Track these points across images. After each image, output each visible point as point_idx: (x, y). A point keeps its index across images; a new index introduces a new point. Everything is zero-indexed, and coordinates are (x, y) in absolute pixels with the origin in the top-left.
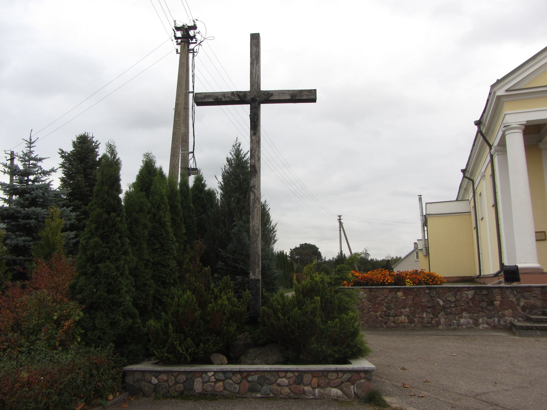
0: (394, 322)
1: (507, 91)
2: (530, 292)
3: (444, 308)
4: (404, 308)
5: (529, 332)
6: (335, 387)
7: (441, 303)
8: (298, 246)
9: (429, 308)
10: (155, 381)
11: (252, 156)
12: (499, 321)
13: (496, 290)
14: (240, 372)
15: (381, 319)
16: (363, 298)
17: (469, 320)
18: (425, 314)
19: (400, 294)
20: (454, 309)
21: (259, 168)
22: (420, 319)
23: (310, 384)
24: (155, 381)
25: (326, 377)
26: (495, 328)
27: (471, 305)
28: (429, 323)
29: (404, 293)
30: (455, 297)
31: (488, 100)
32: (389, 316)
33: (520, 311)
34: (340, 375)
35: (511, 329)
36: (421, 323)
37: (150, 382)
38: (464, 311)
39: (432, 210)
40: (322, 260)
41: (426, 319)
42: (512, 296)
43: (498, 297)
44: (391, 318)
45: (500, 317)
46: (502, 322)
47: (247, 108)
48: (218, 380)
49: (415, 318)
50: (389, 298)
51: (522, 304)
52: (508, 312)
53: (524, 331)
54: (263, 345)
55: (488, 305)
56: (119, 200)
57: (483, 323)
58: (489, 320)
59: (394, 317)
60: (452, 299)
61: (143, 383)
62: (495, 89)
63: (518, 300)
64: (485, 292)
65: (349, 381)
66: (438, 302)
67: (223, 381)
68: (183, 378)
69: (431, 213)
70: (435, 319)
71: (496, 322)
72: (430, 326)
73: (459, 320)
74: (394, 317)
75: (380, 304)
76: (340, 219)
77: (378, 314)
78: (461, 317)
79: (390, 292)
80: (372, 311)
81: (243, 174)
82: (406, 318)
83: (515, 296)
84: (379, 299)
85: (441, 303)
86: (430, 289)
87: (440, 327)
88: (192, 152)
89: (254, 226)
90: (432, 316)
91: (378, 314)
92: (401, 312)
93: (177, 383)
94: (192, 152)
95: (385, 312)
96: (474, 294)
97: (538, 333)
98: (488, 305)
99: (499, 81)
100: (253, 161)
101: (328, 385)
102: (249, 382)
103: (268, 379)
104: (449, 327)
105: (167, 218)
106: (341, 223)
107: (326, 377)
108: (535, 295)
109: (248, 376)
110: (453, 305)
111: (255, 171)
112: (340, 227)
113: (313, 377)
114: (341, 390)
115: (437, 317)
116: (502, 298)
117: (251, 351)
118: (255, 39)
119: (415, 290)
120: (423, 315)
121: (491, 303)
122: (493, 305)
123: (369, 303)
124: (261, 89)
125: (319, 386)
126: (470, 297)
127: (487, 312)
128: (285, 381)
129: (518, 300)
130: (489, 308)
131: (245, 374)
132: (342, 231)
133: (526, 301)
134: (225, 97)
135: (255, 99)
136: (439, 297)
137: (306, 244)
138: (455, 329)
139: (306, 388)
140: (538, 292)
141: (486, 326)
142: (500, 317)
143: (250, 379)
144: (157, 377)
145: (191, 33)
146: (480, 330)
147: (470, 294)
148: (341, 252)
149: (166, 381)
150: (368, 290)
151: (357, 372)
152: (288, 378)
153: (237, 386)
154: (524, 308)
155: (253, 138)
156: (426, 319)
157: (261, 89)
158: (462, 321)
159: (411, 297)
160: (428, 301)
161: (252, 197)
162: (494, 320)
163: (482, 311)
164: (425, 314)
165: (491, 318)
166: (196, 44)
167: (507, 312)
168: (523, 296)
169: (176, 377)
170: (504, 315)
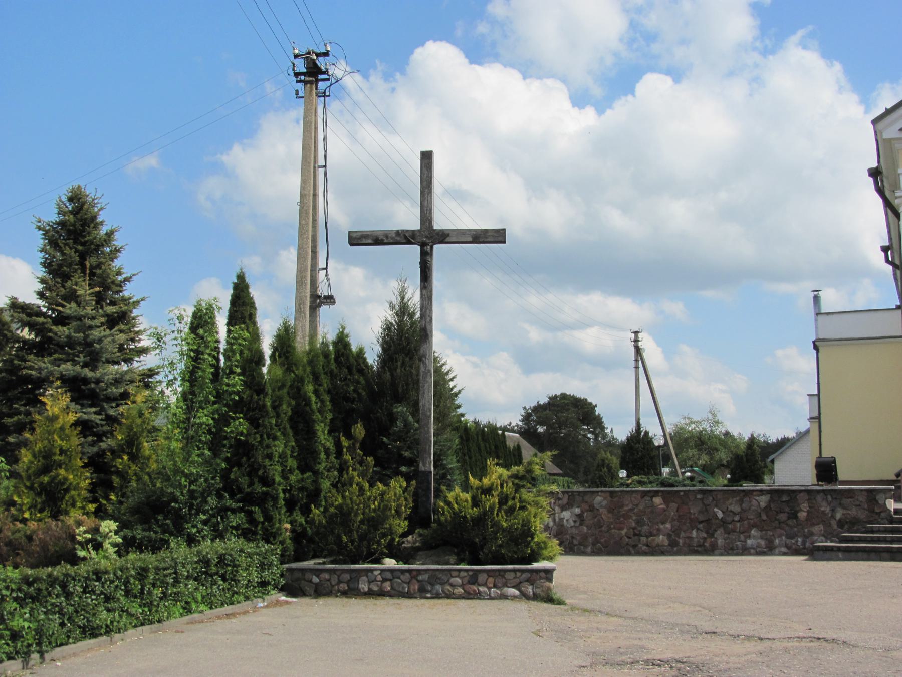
0: (647, 545)
2: (851, 498)
3: (724, 522)
4: (663, 523)
5: (828, 554)
6: (513, 587)
7: (720, 515)
8: (544, 400)
9: (701, 522)
10: (316, 580)
11: (422, 316)
12: (804, 543)
13: (802, 495)
14: (409, 571)
15: (627, 540)
16: (602, 507)
17: (759, 540)
18: (694, 532)
19: (658, 501)
20: (738, 524)
21: (431, 332)
22: (687, 541)
23: (485, 585)
24: (316, 580)
25: (503, 576)
27: (764, 517)
28: (700, 546)
29: (664, 499)
30: (741, 505)
32: (640, 535)
33: (835, 527)
34: (518, 574)
35: (815, 553)
36: (689, 545)
37: (311, 581)
40: (605, 436)
41: (696, 540)
42: (824, 504)
43: (805, 506)
44: (644, 539)
45: (805, 537)
46: (808, 544)
47: (416, 249)
48: (385, 580)
49: (679, 537)
50: (641, 507)
51: (838, 516)
52: (818, 529)
53: (821, 552)
54: (437, 547)
55: (789, 518)
56: (261, 375)
57: (780, 545)
58: (788, 541)
59: (647, 537)
60: (737, 509)
61: (303, 582)
63: (833, 510)
64: (785, 498)
65: (527, 581)
67: (390, 580)
68: (347, 577)
70: (708, 540)
71: (799, 543)
73: (745, 541)
74: (647, 537)
75: (626, 516)
76: (636, 341)
77: (624, 532)
78: (749, 537)
79: (642, 497)
80: (614, 528)
81: (408, 339)
82: (665, 538)
83: (829, 504)
84: (626, 508)
85: (720, 515)
88: (323, 269)
89: (424, 406)
90: (705, 535)
91: (624, 532)
92: (659, 530)
93: (340, 582)
94: (323, 269)
95: (634, 528)
96: (770, 502)
97: (840, 555)
98: (789, 518)
100: (424, 323)
101: (505, 585)
102: (418, 581)
103: (439, 579)
105: (309, 388)
106: (638, 350)
107: (503, 576)
108: (858, 503)
109: (417, 575)
110: (737, 518)
111: (425, 335)
112: (636, 360)
113: (489, 576)
114: (519, 590)
115: (712, 535)
116: (810, 507)
117: (420, 553)
118: (427, 158)
119: (682, 494)
120: (691, 533)
121: (794, 515)
122: (796, 517)
123: (610, 515)
124: (435, 228)
125: (495, 586)
126: (763, 505)
127: (787, 528)
128: (459, 580)
129: (833, 510)
130: (790, 522)
131: (414, 573)
133: (845, 512)
134: (387, 237)
135: (427, 239)
136: (716, 506)
137: (564, 396)
139: (481, 589)
140: (862, 499)
141: (784, 549)
142: (805, 537)
143: (420, 578)
144: (318, 576)
145: (321, 63)
147: (763, 500)
148: (638, 425)
149: (329, 580)
150: (608, 494)
151: (537, 571)
152: (462, 578)
153: (406, 585)
154: (841, 524)
155: (424, 292)
156: (696, 540)
157: (435, 228)
159: (674, 506)
160: (700, 512)
161: (422, 369)
162: (797, 541)
163: (779, 527)
164: (694, 532)
165: (792, 538)
166: (328, 83)
167: (816, 529)
168: (840, 504)
169: (339, 577)
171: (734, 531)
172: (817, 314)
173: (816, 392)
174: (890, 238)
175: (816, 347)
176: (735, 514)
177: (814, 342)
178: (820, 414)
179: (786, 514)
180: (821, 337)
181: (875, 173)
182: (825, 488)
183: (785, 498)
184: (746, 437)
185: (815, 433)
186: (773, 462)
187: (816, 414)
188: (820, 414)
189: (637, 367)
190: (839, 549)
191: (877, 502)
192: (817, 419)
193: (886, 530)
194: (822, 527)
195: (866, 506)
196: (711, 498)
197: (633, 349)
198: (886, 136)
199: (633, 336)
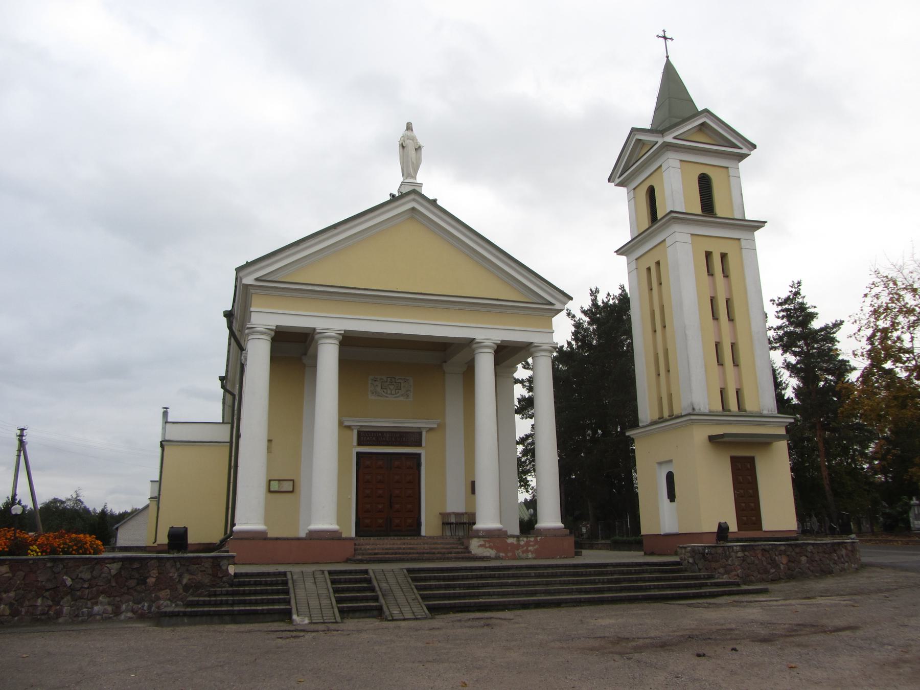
1: (257, 279)
3: (72, 589)
7: (69, 582)
9: (47, 590)
12: (150, 607)
18: (39, 601)
26: (142, 617)
27: (114, 584)
28: (43, 614)
30: (92, 572)
31: (236, 287)
33: (181, 591)
35: (161, 618)
38: (102, 593)
39: (174, 433)
41: (40, 608)
42: (173, 570)
43: (154, 573)
46: (153, 608)
51: (185, 581)
53: (167, 618)
55: (138, 584)
57: (126, 611)
58: (135, 606)
60: (87, 576)
62: (241, 274)
63: (180, 576)
64: (136, 565)
66: (64, 581)
69: (172, 439)
70: (54, 608)
71: (145, 608)
72: (45, 620)
73: (92, 608)
76: (21, 436)
78: (96, 604)
82: (7, 608)
83: (178, 570)
85: (69, 582)
86: (54, 560)
87: (61, 620)
90: (50, 603)
96: (121, 568)
98: (138, 584)
99: (249, 264)
104: (76, 618)
106: (22, 444)
112: (19, 451)
115: (58, 603)
119: (31, 562)
121: (143, 581)
122: (145, 583)
126: (113, 572)
129: (180, 576)
130: (139, 588)
132: (22, 458)
133: (191, 577)
136: (66, 574)
138: (83, 622)
141: (130, 614)
146: (122, 621)
147: (114, 568)
154: (186, 588)
156: (40, 608)
158: (96, 608)
165: (139, 603)
167: (162, 594)
168: (188, 570)
170: (158, 598)
171: (81, 598)
172: (167, 422)
173: (158, 479)
174: (227, 371)
175: (162, 446)
176: (84, 581)
177: (161, 442)
178: (159, 495)
179: (135, 581)
180: (167, 438)
181: (229, 315)
182: (175, 555)
183: (136, 565)
184: (99, 510)
185: (153, 507)
186: (117, 529)
187: (156, 494)
188: (159, 495)
189: (19, 456)
190: (185, 614)
191: (220, 567)
192: (156, 499)
193: (228, 594)
194: (168, 591)
195: (210, 572)
196: (61, 566)
197: (17, 442)
198: (245, 281)
199: (19, 432)
